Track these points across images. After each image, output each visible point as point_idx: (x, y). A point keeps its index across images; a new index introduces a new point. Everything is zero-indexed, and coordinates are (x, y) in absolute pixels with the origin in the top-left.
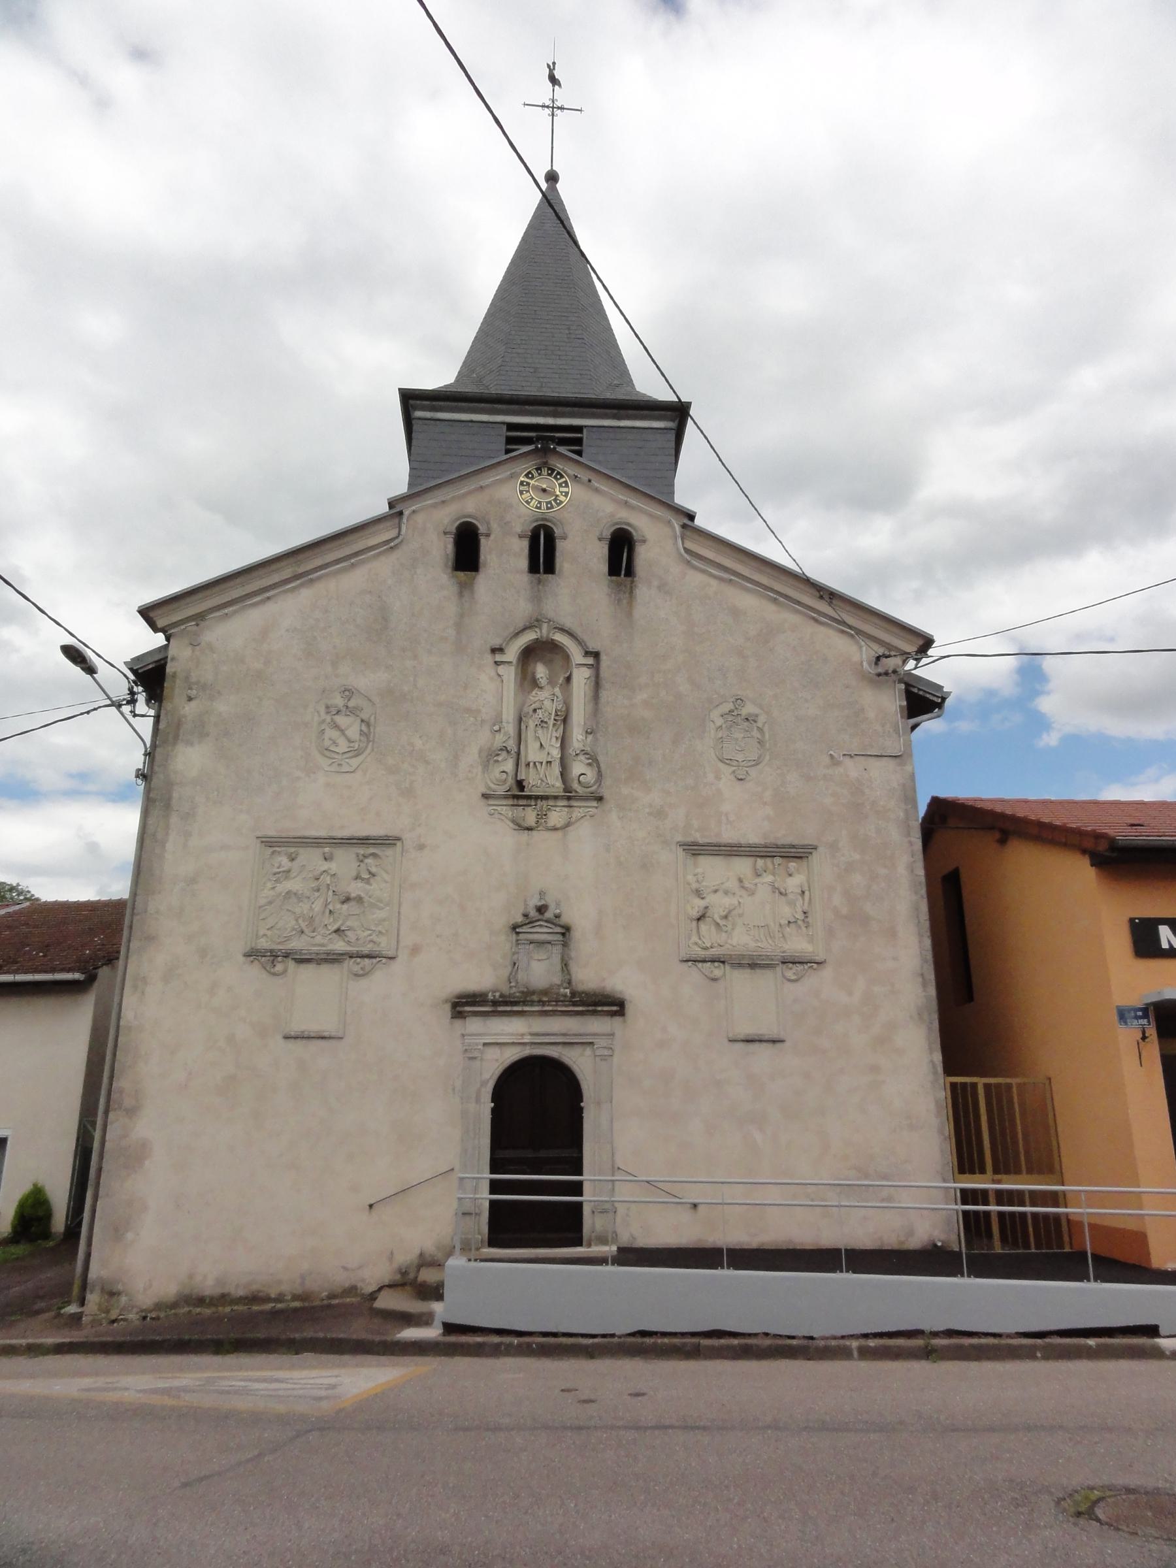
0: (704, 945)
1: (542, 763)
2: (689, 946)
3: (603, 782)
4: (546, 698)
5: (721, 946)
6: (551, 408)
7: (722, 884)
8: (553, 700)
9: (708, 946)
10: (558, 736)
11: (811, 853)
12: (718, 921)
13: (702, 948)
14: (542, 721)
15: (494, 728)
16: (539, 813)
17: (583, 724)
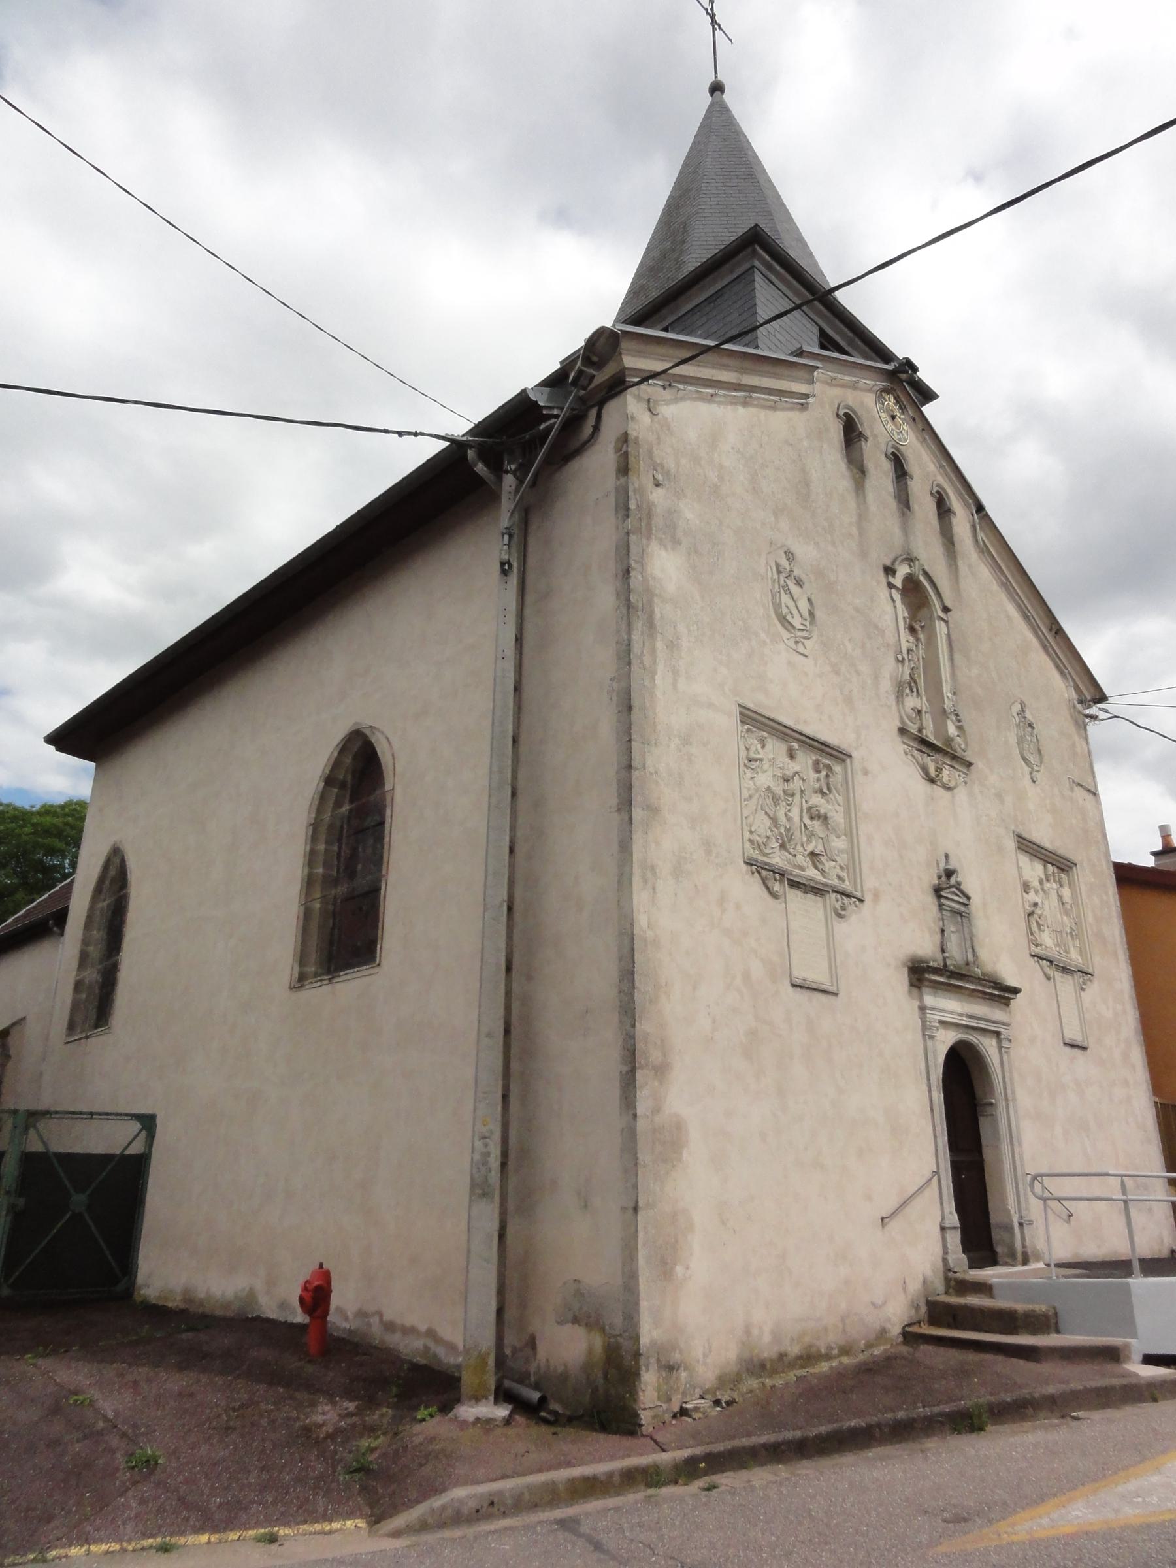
6: (850, 334)
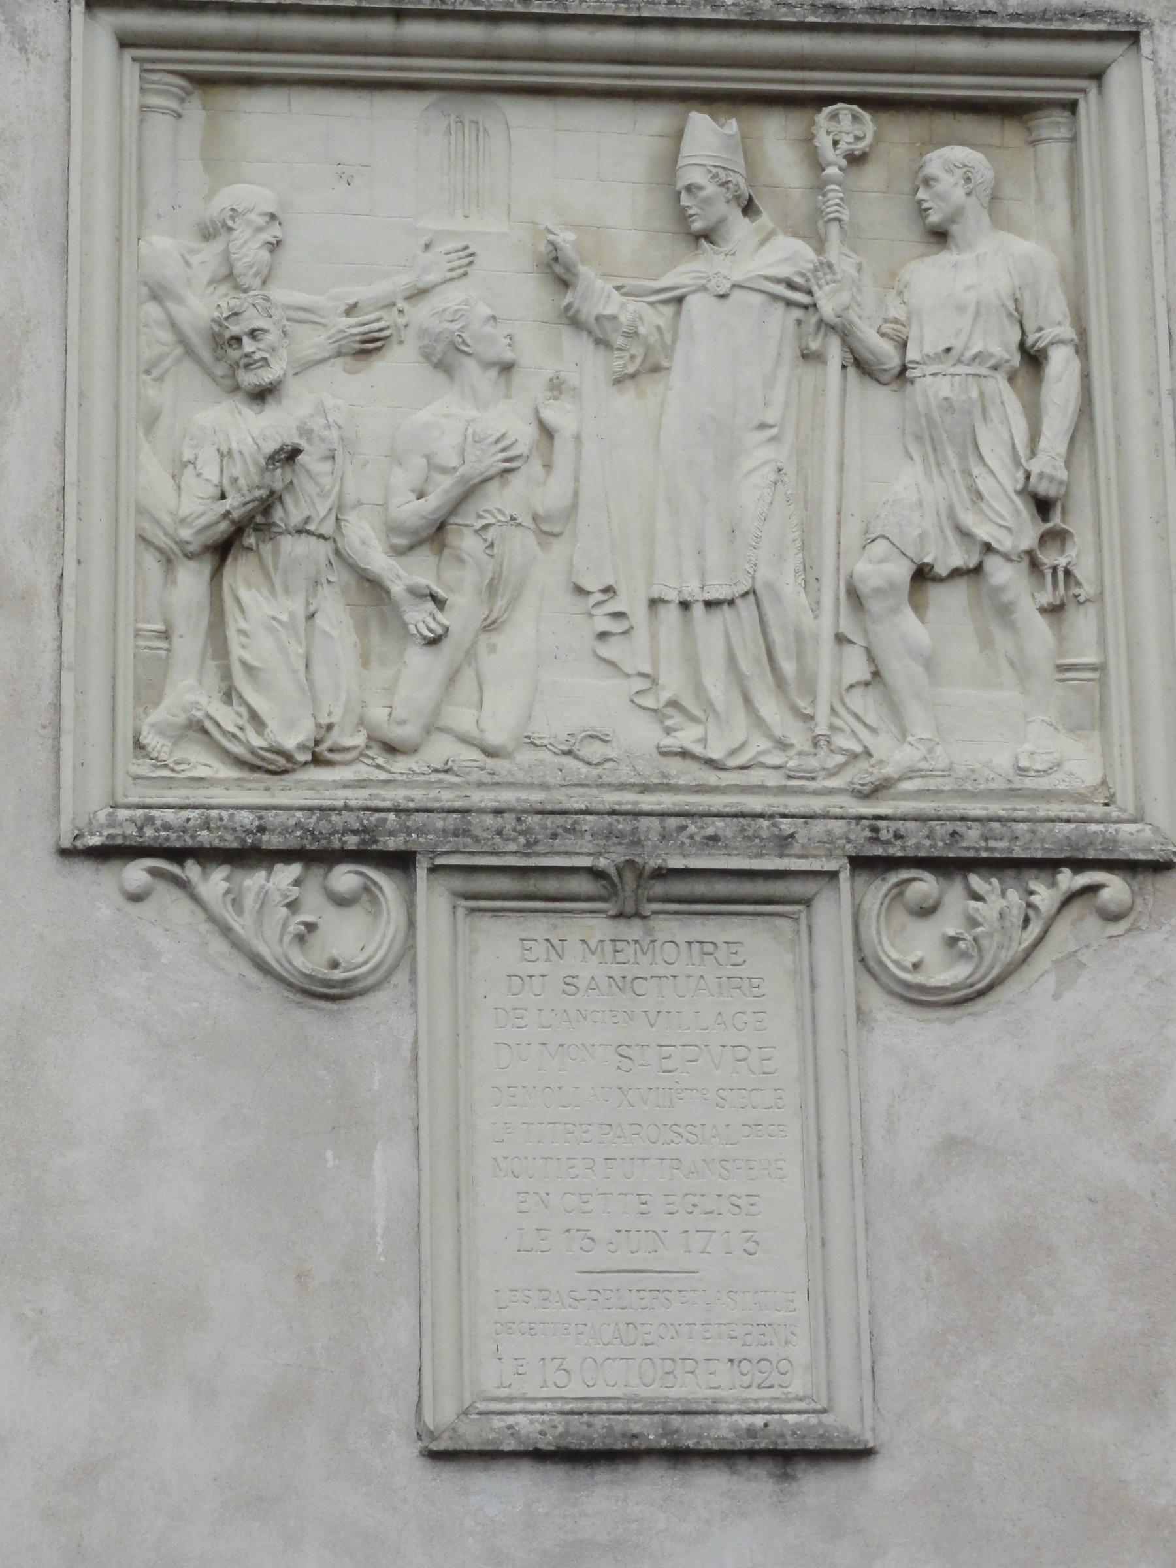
0: (257, 741)
2: (139, 746)
5: (391, 749)
7: (419, 294)
9: (290, 743)
11: (1097, 75)
12: (379, 561)
13: (240, 762)
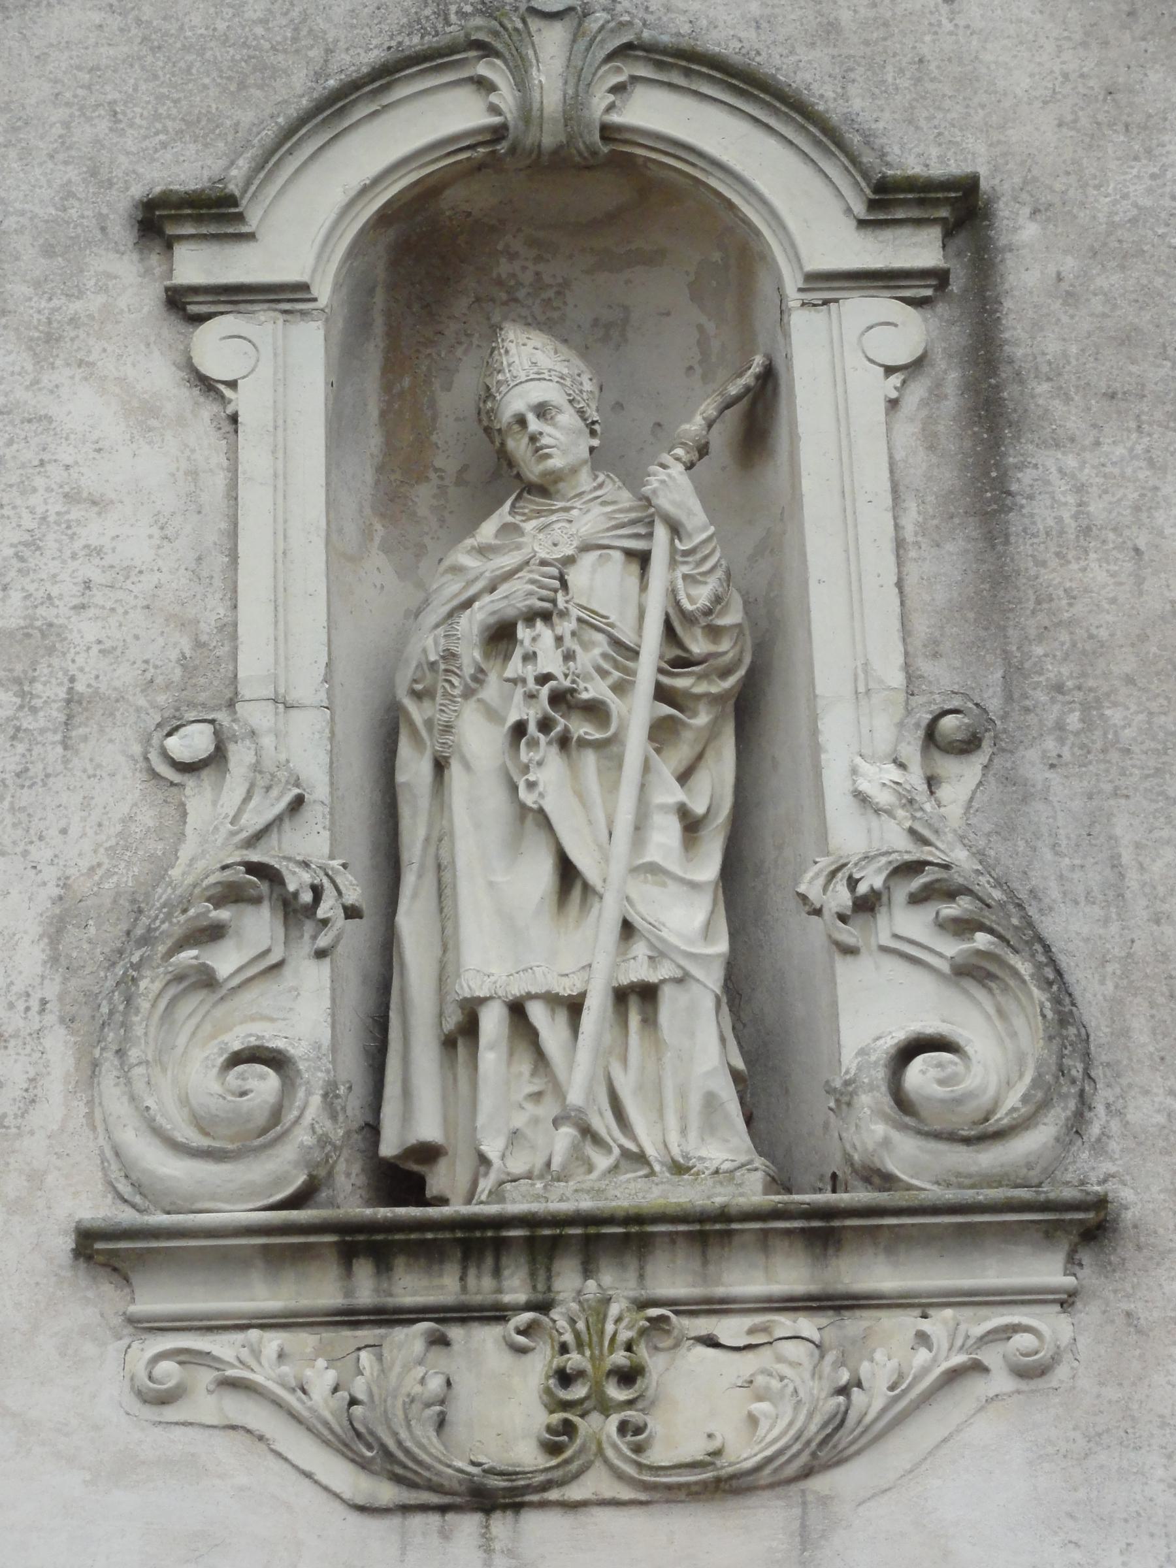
1: (574, 1007)
3: (1102, 1096)
4: (586, 548)
8: (642, 559)
10: (699, 808)
14: (559, 699)
15: (172, 743)
16: (575, 1360)
17: (897, 679)
